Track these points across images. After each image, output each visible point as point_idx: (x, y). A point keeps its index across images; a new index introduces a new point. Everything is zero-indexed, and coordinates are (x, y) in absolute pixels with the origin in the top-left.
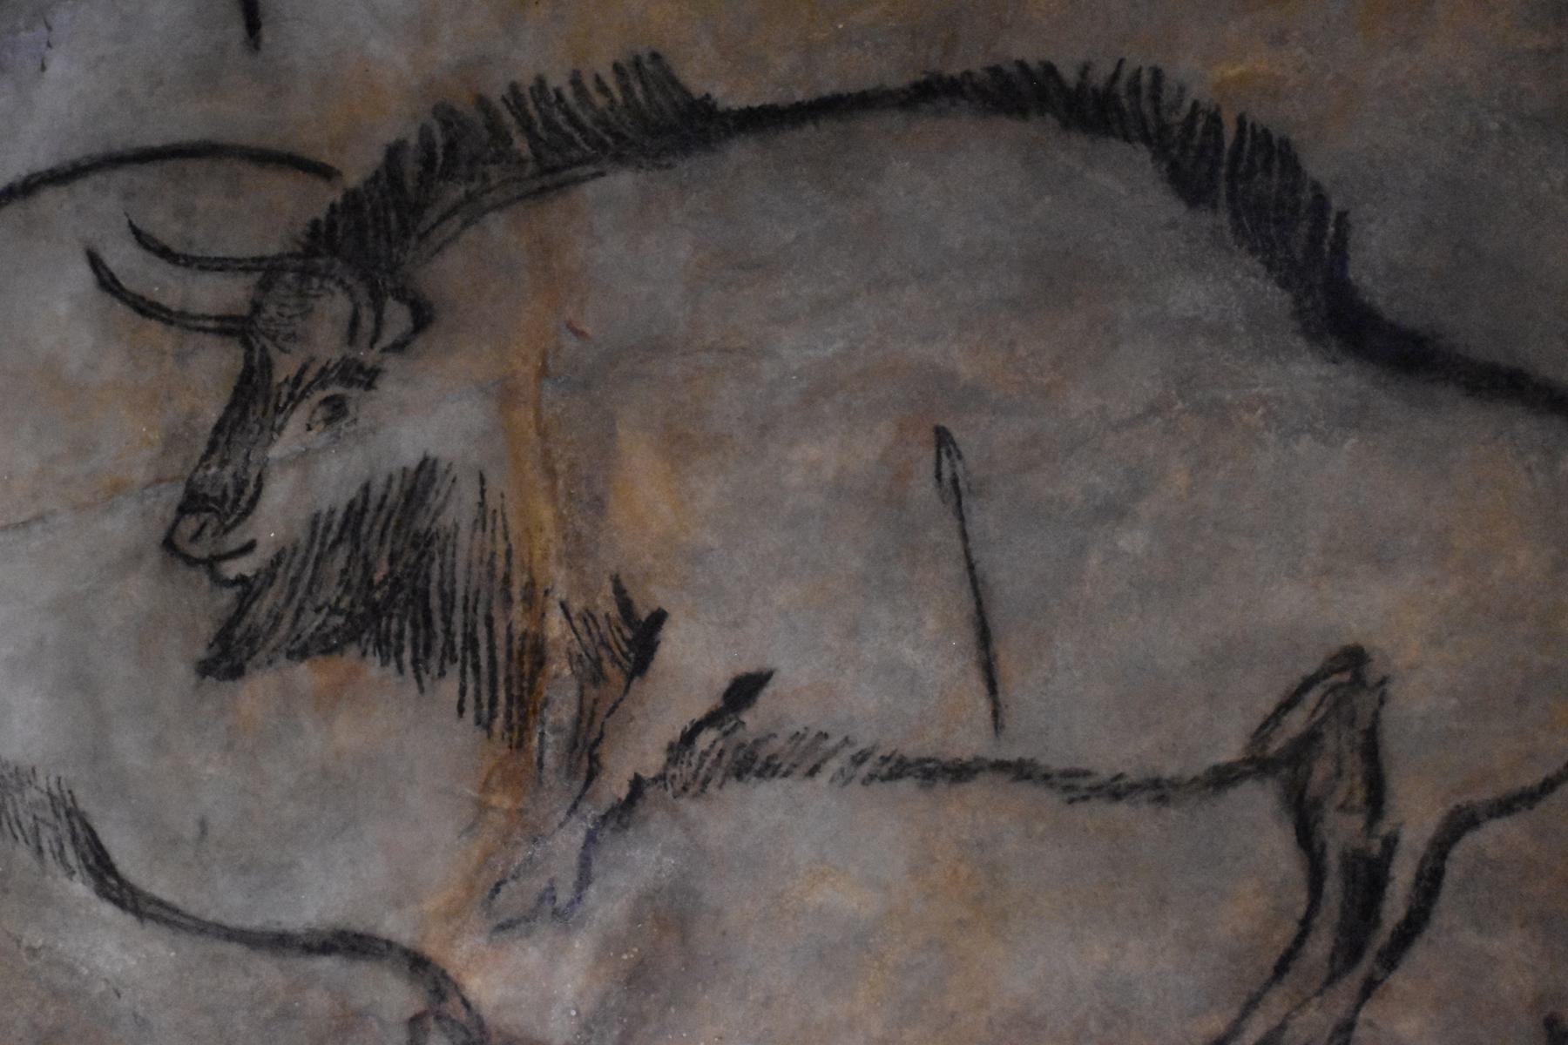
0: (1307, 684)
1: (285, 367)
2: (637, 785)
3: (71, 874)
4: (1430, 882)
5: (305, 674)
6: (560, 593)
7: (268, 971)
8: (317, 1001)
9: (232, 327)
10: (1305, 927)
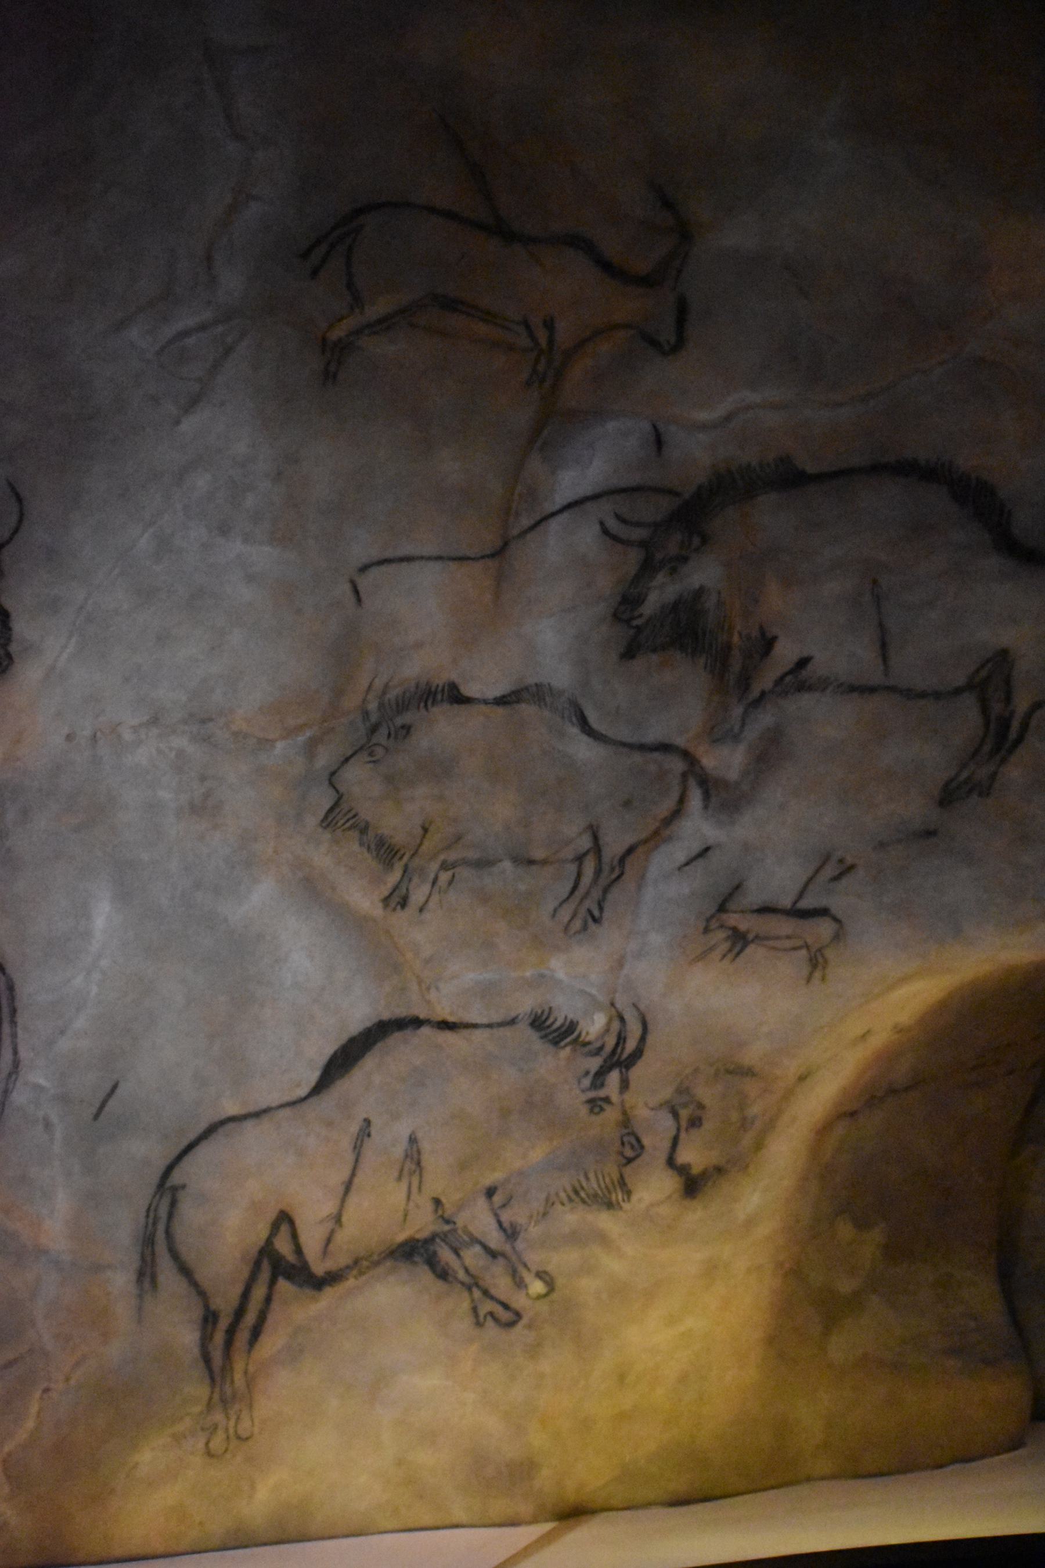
0: (988, 661)
1: (659, 556)
2: (763, 694)
3: (573, 724)
4: (1025, 726)
5: (655, 658)
6: (738, 628)
7: (637, 758)
8: (653, 768)
9: (643, 544)
10: (983, 741)
